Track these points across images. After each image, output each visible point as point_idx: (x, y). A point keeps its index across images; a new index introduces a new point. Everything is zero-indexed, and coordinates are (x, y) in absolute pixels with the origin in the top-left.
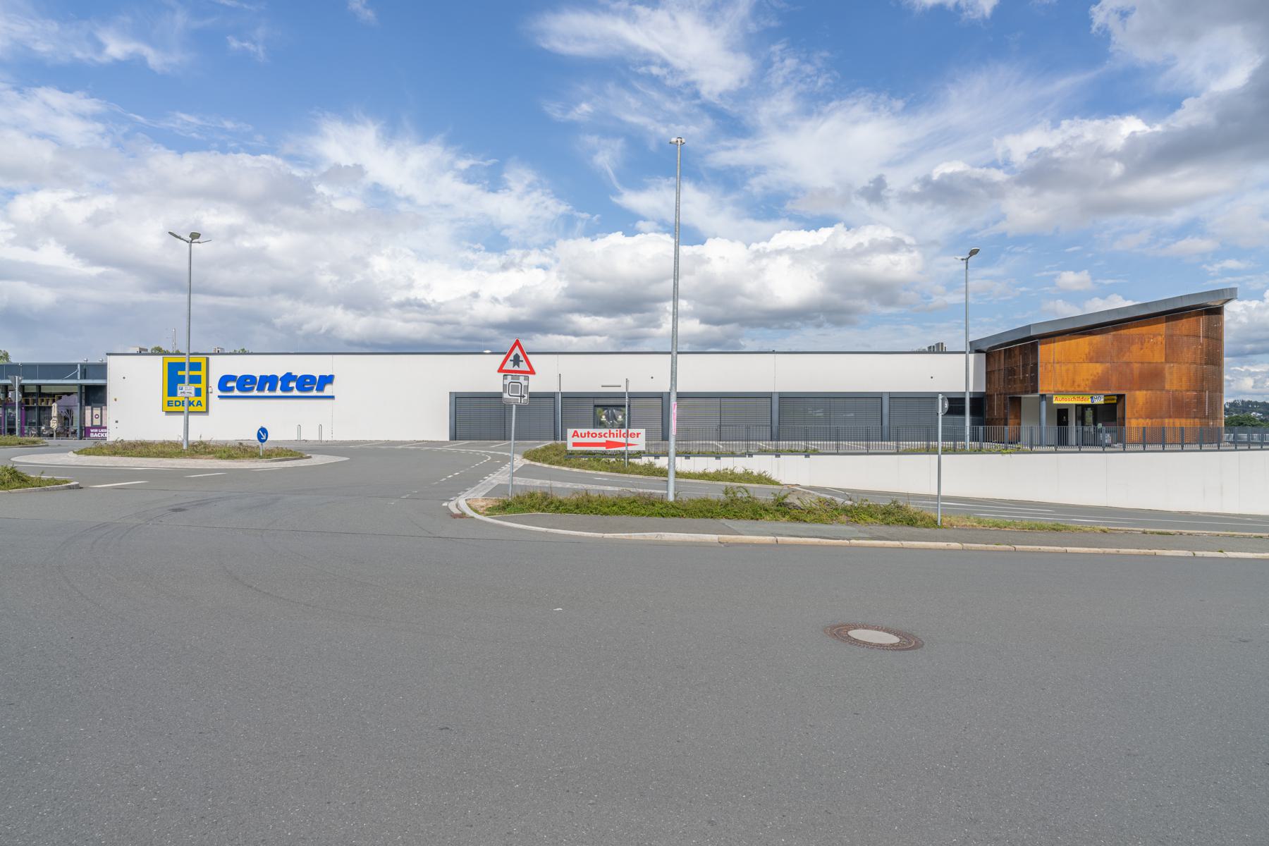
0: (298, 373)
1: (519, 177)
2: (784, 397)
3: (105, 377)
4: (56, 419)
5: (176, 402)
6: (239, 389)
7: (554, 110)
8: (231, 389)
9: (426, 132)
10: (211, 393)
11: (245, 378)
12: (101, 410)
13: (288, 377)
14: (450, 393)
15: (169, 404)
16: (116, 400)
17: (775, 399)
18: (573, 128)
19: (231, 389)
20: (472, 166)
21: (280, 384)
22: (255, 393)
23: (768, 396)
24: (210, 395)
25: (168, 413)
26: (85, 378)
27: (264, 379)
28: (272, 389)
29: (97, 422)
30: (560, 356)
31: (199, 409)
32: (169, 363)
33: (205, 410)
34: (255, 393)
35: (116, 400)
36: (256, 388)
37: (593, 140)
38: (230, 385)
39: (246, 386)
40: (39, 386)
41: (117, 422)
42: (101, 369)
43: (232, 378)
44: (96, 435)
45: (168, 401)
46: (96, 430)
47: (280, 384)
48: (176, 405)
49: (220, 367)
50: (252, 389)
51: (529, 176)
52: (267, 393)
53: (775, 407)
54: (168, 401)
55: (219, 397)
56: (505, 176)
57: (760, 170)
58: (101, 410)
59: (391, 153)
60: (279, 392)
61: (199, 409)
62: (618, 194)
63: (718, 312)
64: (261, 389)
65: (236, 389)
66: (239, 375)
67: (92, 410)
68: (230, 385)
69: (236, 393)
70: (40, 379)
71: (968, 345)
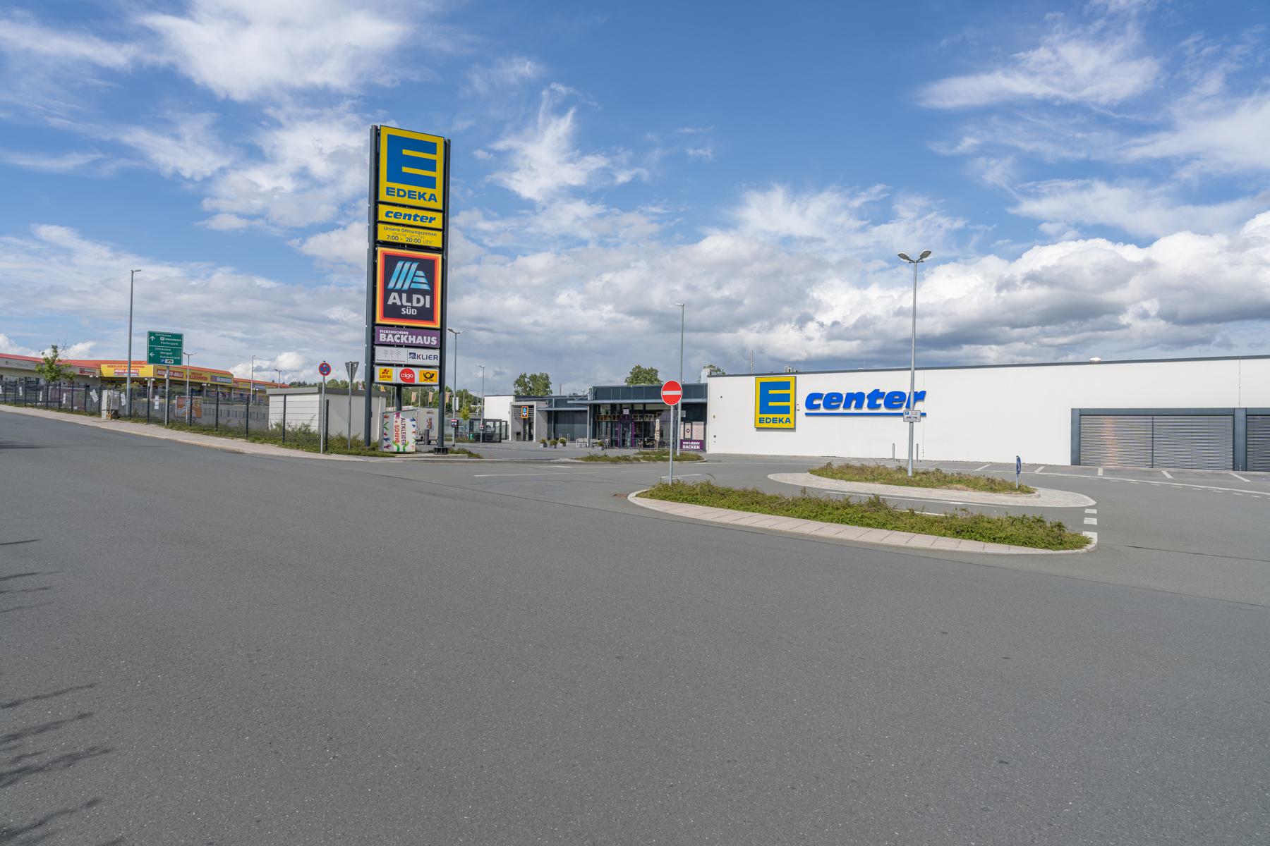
0: (886, 389)
1: (909, 207)
2: (1251, 414)
3: (706, 397)
4: (659, 433)
5: (767, 419)
6: (826, 407)
7: (940, 148)
8: (818, 407)
9: (821, 187)
10: (798, 410)
11: (830, 395)
12: (692, 425)
13: (876, 394)
14: (1072, 409)
15: (761, 421)
16: (714, 417)
17: (1241, 417)
18: (962, 160)
19: (818, 407)
20: (865, 203)
21: (866, 401)
22: (841, 410)
23: (1231, 413)
24: (797, 412)
25: (759, 429)
26: (596, 399)
27: (850, 397)
28: (859, 406)
29: (688, 436)
30: (1243, 361)
31: (787, 425)
32: (761, 383)
33: (793, 427)
34: (841, 410)
35: (714, 417)
36: (842, 405)
37: (981, 161)
38: (816, 402)
39: (833, 404)
40: (644, 404)
41: (715, 436)
42: (701, 390)
43: (819, 396)
44: (687, 447)
45: (760, 418)
46: (687, 443)
47: (866, 401)
48: (767, 422)
49: (806, 385)
50: (837, 407)
51: (920, 201)
52: (853, 410)
53: (1241, 428)
54: (760, 418)
55: (807, 414)
56: (896, 206)
57: (1189, 159)
58: (692, 425)
59: (794, 207)
60: (865, 409)
61: (787, 425)
62: (1015, 203)
63: (1185, 309)
64: (847, 406)
65: (822, 406)
66: (825, 392)
67: (684, 425)
68: (816, 402)
69: (822, 410)
70: (613, 399)
71: (200, 372)
